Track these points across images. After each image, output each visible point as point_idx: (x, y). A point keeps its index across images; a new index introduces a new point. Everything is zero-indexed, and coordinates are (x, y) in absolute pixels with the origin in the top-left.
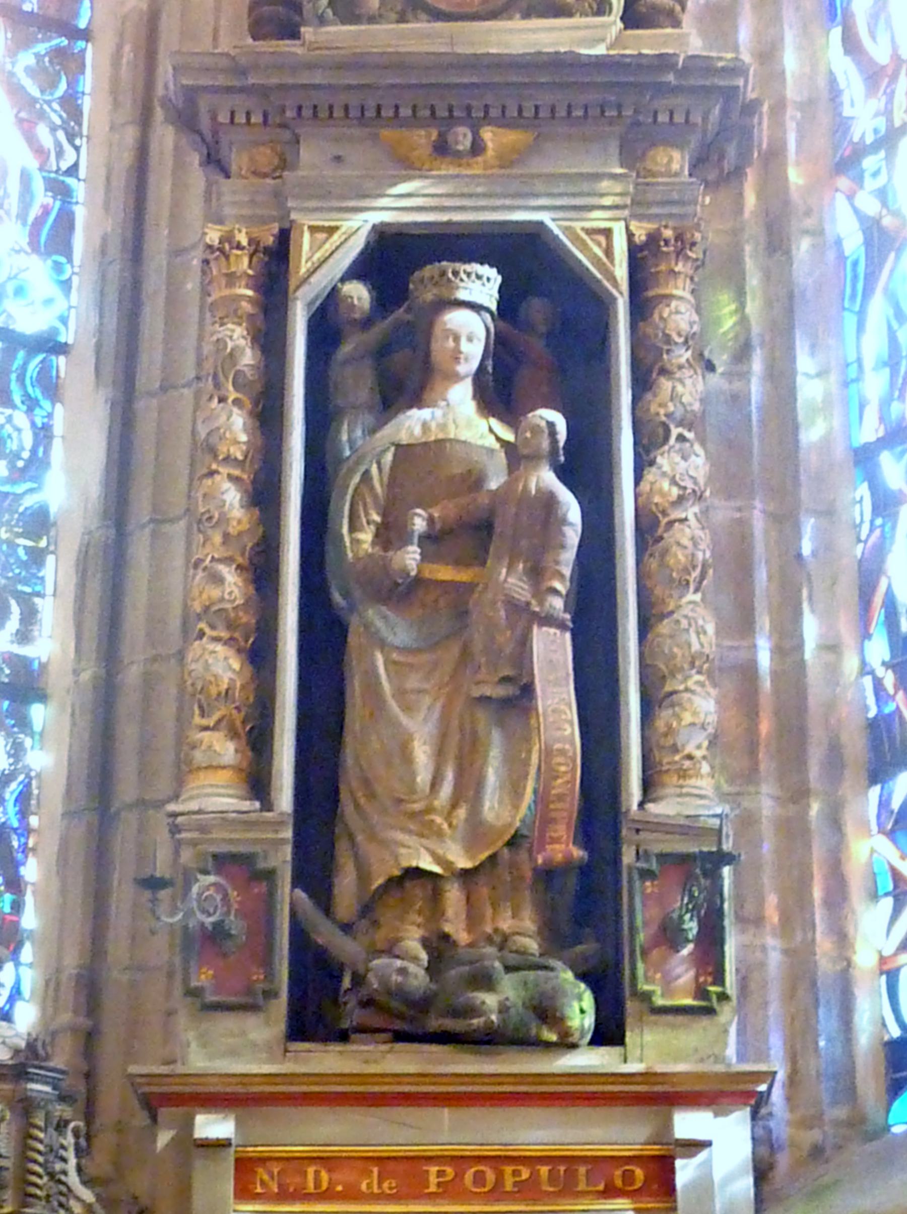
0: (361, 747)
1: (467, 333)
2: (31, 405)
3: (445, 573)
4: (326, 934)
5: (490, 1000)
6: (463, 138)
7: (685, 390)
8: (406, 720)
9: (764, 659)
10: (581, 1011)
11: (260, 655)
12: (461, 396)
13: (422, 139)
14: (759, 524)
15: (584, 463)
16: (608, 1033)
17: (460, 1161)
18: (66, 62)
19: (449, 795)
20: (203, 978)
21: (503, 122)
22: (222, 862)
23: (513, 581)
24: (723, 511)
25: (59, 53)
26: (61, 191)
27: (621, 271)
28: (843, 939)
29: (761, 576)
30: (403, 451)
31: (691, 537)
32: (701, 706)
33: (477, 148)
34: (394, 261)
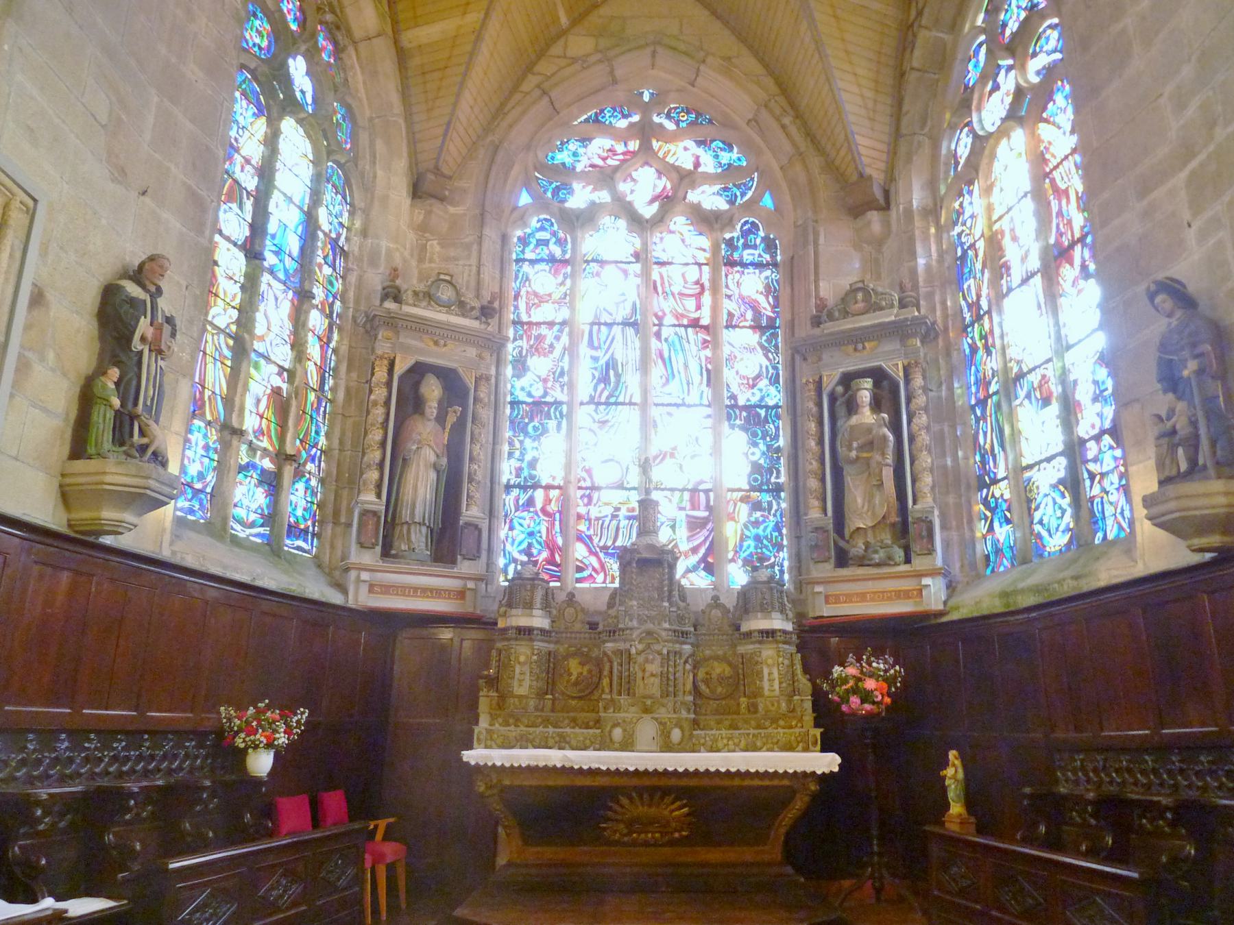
0: (848, 499)
1: (865, 396)
2: (774, 422)
3: (865, 455)
4: (842, 543)
5: (876, 556)
6: (860, 346)
7: (921, 400)
8: (856, 495)
9: (949, 463)
10: (899, 554)
11: (823, 480)
12: (867, 411)
13: (850, 348)
14: (946, 429)
15: (896, 428)
16: (908, 561)
17: (874, 593)
18: (774, 335)
19: (867, 506)
20: (815, 555)
21: (869, 340)
22: (816, 529)
23: (878, 458)
24: (936, 428)
25: (772, 334)
26: (775, 368)
27: (901, 374)
28: (972, 531)
29: (948, 442)
30: (852, 427)
31: (924, 438)
32: (927, 480)
33: (864, 348)
34: (848, 380)
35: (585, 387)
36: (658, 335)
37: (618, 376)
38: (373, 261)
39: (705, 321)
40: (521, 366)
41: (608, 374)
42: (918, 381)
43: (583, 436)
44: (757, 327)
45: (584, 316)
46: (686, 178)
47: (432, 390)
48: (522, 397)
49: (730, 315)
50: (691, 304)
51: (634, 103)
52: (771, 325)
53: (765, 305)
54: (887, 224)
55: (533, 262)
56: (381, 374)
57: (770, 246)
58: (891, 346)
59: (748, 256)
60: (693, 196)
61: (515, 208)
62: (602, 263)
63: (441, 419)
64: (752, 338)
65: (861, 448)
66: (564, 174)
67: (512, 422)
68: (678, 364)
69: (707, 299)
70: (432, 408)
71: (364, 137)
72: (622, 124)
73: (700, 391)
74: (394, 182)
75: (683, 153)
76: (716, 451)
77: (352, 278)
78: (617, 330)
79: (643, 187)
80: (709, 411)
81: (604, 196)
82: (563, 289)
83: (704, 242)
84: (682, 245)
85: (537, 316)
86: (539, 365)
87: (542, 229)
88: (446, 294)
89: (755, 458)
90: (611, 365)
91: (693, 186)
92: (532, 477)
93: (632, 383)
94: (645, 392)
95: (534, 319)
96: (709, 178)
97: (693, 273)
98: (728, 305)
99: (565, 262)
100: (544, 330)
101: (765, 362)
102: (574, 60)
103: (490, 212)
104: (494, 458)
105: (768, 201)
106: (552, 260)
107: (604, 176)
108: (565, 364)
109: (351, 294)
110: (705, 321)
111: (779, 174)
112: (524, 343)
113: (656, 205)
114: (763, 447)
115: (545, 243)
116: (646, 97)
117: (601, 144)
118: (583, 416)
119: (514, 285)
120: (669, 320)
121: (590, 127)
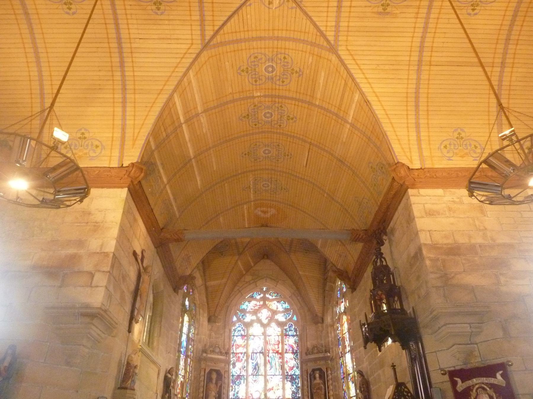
7: (330, 377)
18: (297, 355)
35: (250, 371)
36: (268, 356)
37: (258, 367)
38: (200, 342)
39: (280, 351)
40: (234, 365)
41: (256, 367)
42: (329, 372)
43: (250, 384)
44: (293, 353)
45: (250, 351)
46: (274, 313)
47: (214, 376)
48: (234, 374)
49: (286, 350)
50: (276, 346)
51: (261, 291)
52: (296, 352)
53: (295, 346)
54: (322, 327)
55: (237, 336)
56: (202, 373)
57: (296, 330)
58: (323, 362)
59: (290, 333)
60: (276, 317)
61: (233, 322)
62: (254, 336)
63: (216, 384)
64: (292, 356)
65: (317, 389)
66: (244, 311)
67: (232, 381)
68: (273, 364)
69: (280, 345)
70: (214, 381)
71: (198, 309)
72: (258, 297)
73: (279, 372)
74: (204, 319)
75: (274, 305)
76: (284, 388)
77: (195, 347)
78: (258, 354)
79: (264, 314)
80: (281, 377)
81: (254, 318)
82: (244, 343)
83: (280, 329)
84: (274, 331)
85: (238, 351)
86: (239, 365)
87: (239, 327)
88: (217, 350)
89: (293, 390)
90: (257, 364)
91: (276, 314)
92: (237, 396)
93: (262, 368)
94: (265, 372)
95: (237, 352)
96: (280, 312)
97: (277, 338)
98: (286, 347)
99: (245, 336)
100: (240, 355)
101: (295, 363)
102: (247, 282)
103: (227, 324)
104: (228, 392)
105: (295, 318)
106: (242, 335)
107: (255, 312)
108: (245, 365)
109: (195, 351)
110: (280, 351)
111: (297, 311)
112: (235, 359)
113: (267, 320)
114: (295, 386)
115: (240, 331)
116: (264, 289)
117: (253, 302)
118: (251, 379)
119: (233, 342)
120: (271, 351)
121: (250, 299)
